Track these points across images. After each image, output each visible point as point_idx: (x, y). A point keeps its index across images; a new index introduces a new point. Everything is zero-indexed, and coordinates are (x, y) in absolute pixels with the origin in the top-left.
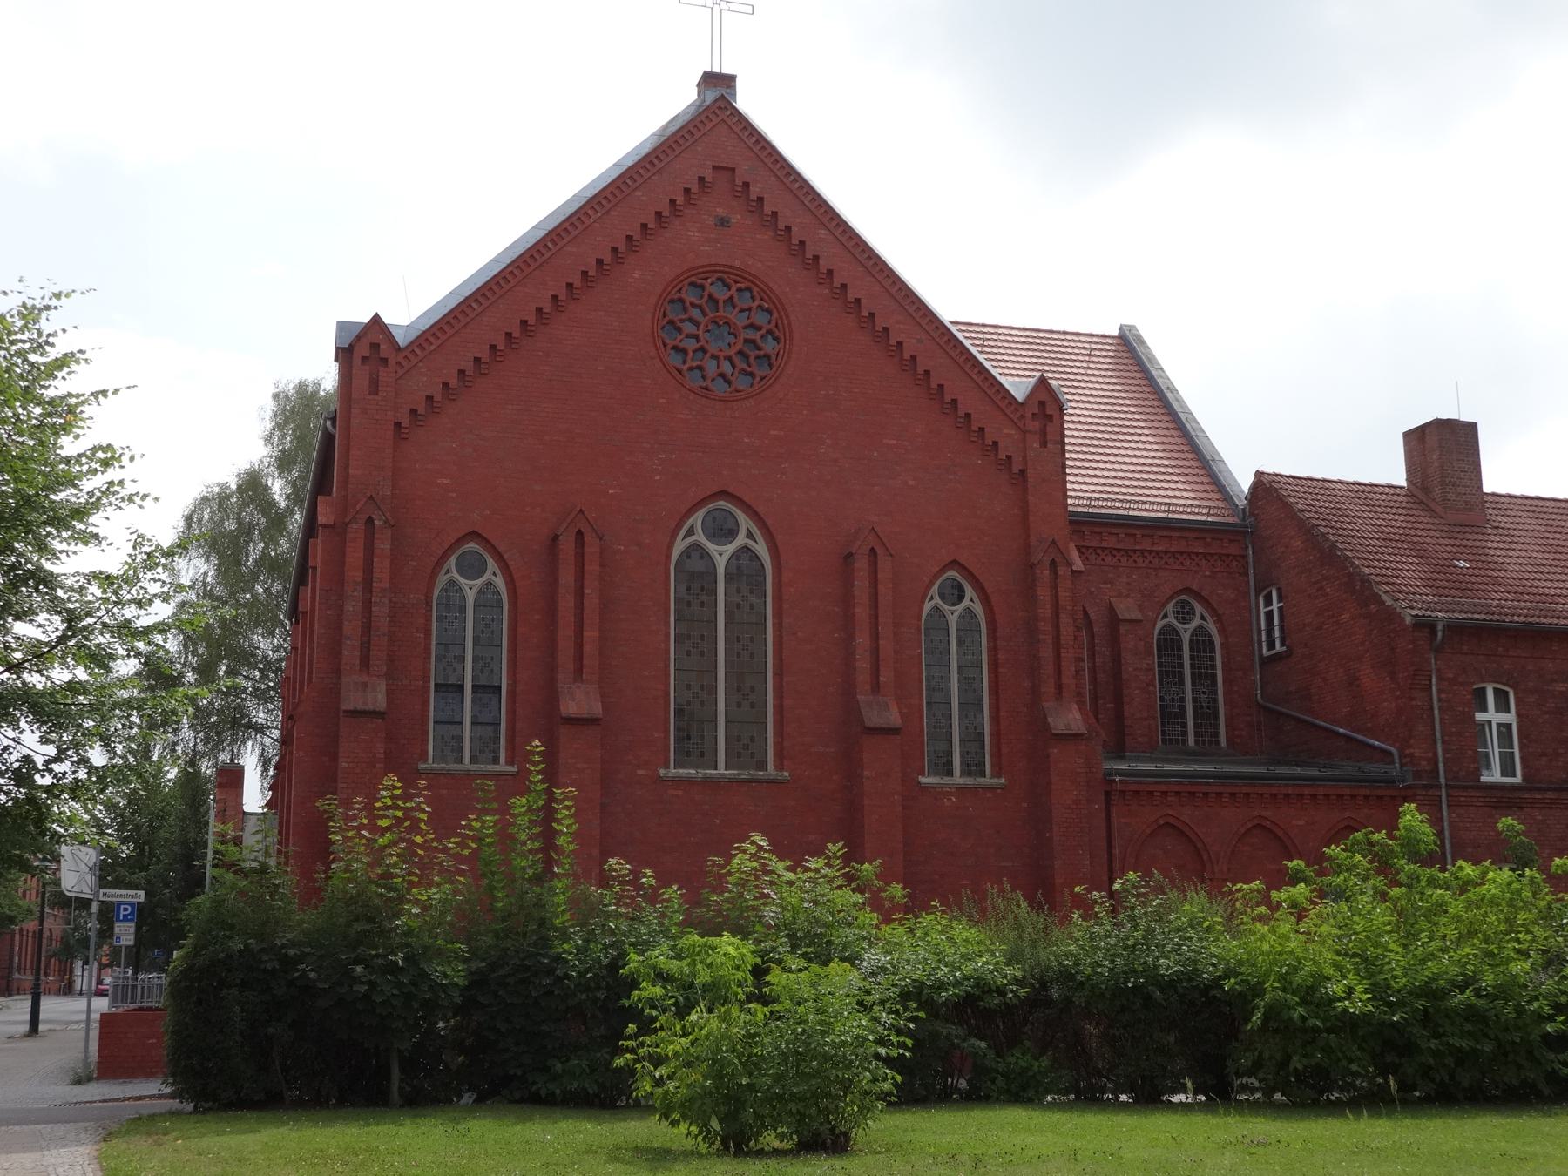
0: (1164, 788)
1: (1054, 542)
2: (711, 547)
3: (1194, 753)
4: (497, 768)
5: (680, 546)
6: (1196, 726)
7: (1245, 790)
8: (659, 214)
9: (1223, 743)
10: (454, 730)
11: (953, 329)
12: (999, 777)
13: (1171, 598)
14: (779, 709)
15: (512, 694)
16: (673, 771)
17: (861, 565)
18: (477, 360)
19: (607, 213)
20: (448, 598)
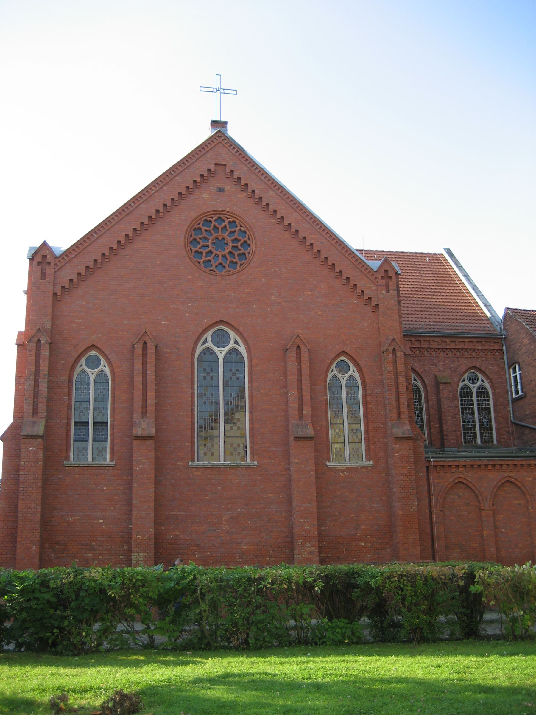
0: (457, 464)
1: (394, 339)
2: (216, 349)
3: (480, 447)
4: (104, 463)
5: (199, 349)
6: (481, 434)
7: (500, 463)
8: (187, 187)
9: (495, 442)
10: (83, 444)
11: (358, 253)
12: (370, 461)
13: (466, 372)
14: (252, 429)
15: (113, 426)
16: (196, 463)
17: (293, 354)
18: (95, 261)
19: (161, 188)
20: (81, 378)
